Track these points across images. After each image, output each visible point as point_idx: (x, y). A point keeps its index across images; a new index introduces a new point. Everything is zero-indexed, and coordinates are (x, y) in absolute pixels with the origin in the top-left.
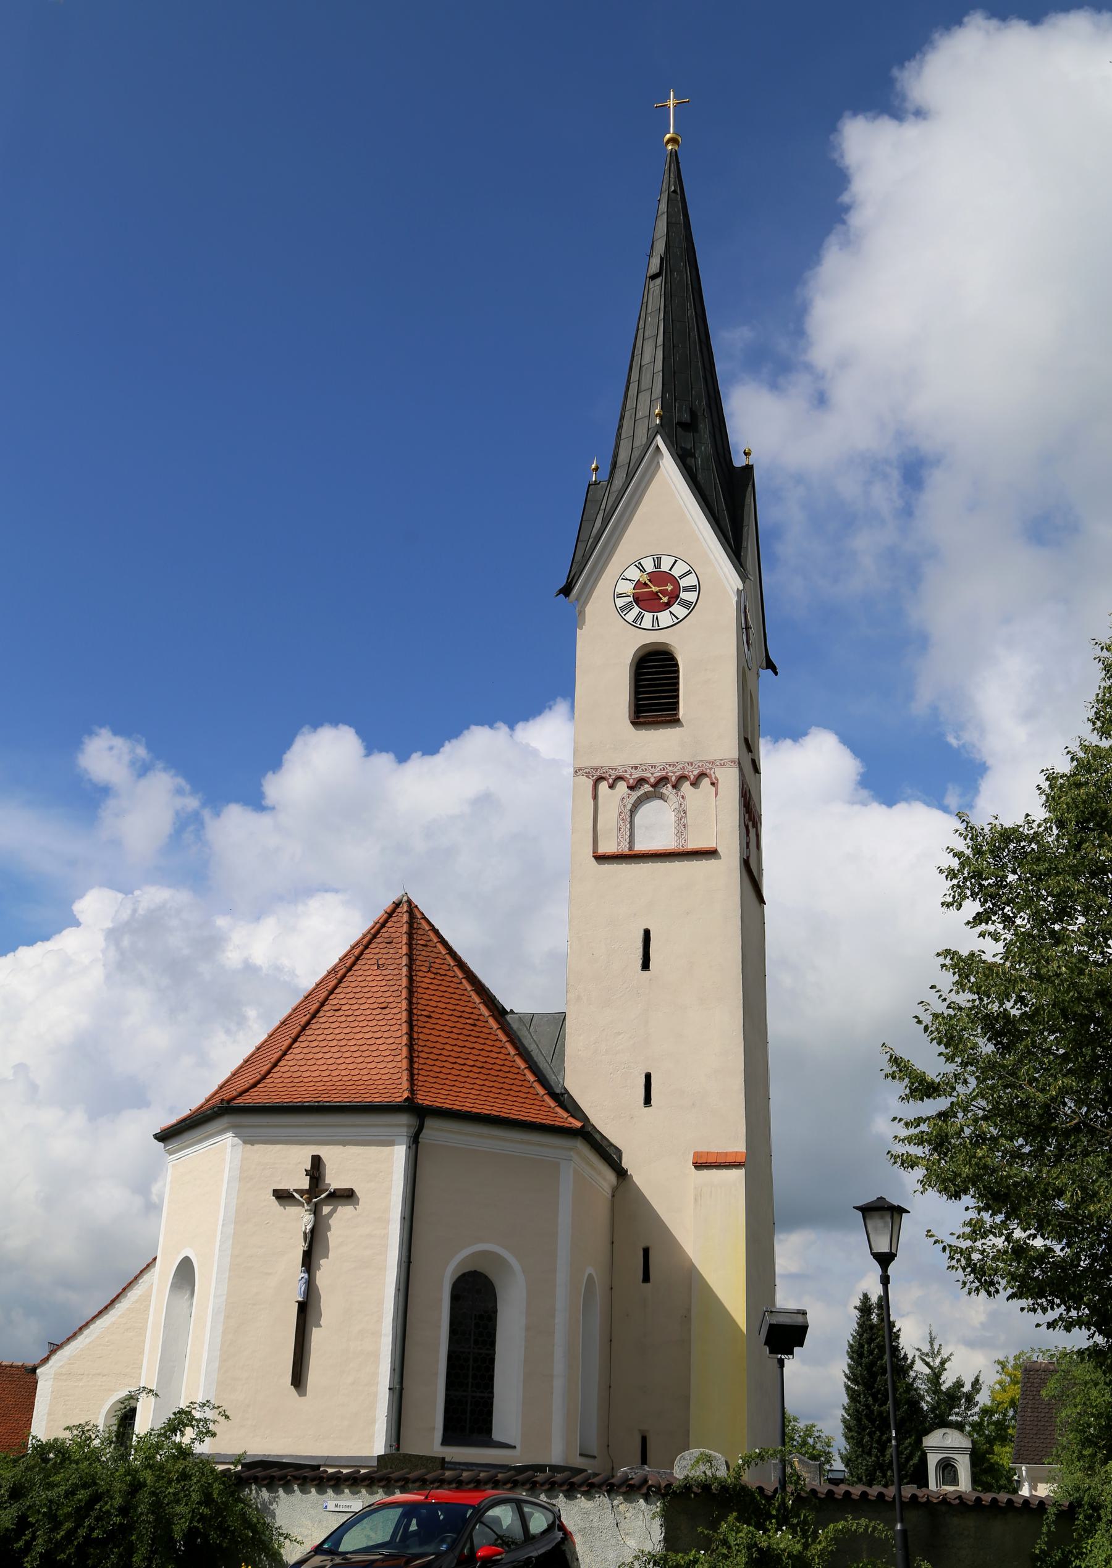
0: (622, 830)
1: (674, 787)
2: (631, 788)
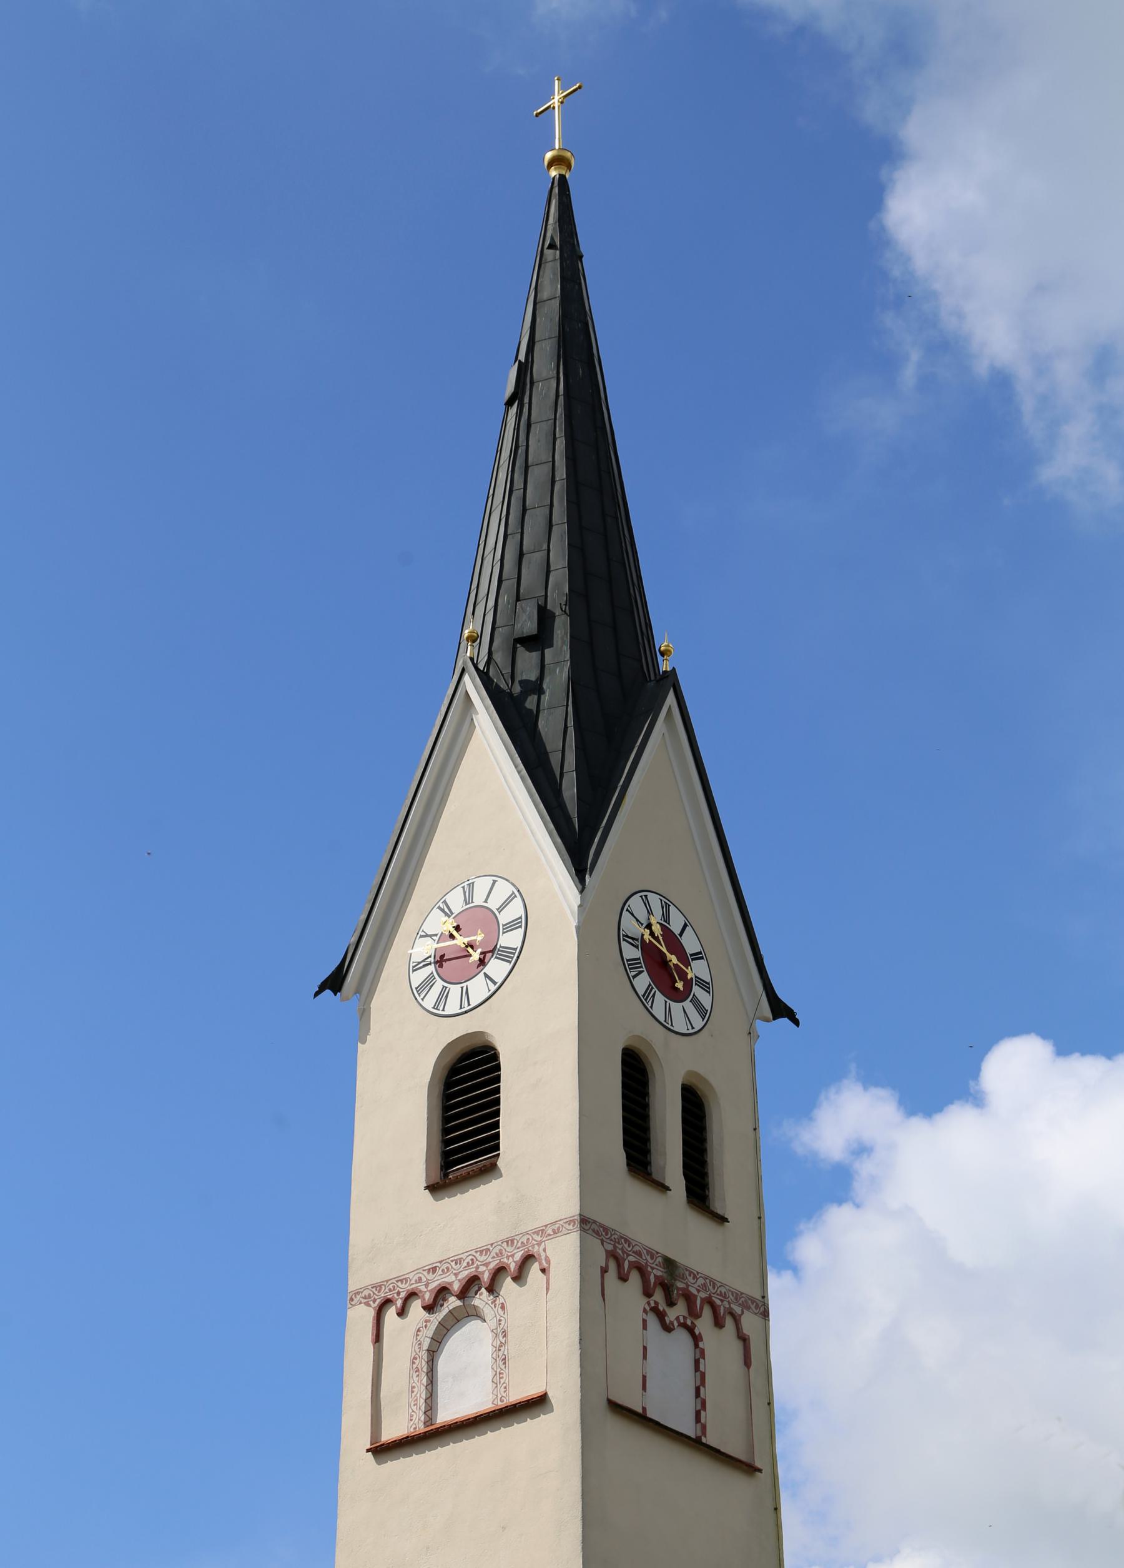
0: (416, 1390)
1: (491, 1290)
2: (430, 1308)
